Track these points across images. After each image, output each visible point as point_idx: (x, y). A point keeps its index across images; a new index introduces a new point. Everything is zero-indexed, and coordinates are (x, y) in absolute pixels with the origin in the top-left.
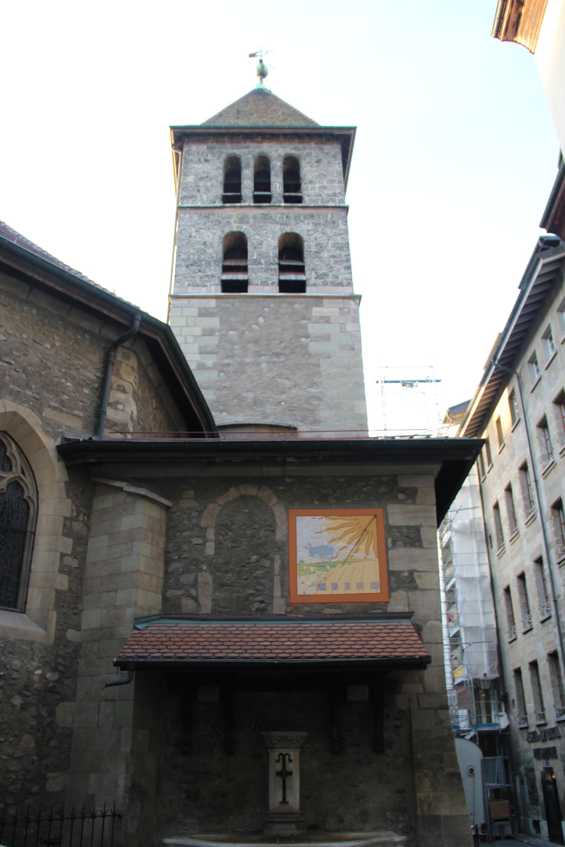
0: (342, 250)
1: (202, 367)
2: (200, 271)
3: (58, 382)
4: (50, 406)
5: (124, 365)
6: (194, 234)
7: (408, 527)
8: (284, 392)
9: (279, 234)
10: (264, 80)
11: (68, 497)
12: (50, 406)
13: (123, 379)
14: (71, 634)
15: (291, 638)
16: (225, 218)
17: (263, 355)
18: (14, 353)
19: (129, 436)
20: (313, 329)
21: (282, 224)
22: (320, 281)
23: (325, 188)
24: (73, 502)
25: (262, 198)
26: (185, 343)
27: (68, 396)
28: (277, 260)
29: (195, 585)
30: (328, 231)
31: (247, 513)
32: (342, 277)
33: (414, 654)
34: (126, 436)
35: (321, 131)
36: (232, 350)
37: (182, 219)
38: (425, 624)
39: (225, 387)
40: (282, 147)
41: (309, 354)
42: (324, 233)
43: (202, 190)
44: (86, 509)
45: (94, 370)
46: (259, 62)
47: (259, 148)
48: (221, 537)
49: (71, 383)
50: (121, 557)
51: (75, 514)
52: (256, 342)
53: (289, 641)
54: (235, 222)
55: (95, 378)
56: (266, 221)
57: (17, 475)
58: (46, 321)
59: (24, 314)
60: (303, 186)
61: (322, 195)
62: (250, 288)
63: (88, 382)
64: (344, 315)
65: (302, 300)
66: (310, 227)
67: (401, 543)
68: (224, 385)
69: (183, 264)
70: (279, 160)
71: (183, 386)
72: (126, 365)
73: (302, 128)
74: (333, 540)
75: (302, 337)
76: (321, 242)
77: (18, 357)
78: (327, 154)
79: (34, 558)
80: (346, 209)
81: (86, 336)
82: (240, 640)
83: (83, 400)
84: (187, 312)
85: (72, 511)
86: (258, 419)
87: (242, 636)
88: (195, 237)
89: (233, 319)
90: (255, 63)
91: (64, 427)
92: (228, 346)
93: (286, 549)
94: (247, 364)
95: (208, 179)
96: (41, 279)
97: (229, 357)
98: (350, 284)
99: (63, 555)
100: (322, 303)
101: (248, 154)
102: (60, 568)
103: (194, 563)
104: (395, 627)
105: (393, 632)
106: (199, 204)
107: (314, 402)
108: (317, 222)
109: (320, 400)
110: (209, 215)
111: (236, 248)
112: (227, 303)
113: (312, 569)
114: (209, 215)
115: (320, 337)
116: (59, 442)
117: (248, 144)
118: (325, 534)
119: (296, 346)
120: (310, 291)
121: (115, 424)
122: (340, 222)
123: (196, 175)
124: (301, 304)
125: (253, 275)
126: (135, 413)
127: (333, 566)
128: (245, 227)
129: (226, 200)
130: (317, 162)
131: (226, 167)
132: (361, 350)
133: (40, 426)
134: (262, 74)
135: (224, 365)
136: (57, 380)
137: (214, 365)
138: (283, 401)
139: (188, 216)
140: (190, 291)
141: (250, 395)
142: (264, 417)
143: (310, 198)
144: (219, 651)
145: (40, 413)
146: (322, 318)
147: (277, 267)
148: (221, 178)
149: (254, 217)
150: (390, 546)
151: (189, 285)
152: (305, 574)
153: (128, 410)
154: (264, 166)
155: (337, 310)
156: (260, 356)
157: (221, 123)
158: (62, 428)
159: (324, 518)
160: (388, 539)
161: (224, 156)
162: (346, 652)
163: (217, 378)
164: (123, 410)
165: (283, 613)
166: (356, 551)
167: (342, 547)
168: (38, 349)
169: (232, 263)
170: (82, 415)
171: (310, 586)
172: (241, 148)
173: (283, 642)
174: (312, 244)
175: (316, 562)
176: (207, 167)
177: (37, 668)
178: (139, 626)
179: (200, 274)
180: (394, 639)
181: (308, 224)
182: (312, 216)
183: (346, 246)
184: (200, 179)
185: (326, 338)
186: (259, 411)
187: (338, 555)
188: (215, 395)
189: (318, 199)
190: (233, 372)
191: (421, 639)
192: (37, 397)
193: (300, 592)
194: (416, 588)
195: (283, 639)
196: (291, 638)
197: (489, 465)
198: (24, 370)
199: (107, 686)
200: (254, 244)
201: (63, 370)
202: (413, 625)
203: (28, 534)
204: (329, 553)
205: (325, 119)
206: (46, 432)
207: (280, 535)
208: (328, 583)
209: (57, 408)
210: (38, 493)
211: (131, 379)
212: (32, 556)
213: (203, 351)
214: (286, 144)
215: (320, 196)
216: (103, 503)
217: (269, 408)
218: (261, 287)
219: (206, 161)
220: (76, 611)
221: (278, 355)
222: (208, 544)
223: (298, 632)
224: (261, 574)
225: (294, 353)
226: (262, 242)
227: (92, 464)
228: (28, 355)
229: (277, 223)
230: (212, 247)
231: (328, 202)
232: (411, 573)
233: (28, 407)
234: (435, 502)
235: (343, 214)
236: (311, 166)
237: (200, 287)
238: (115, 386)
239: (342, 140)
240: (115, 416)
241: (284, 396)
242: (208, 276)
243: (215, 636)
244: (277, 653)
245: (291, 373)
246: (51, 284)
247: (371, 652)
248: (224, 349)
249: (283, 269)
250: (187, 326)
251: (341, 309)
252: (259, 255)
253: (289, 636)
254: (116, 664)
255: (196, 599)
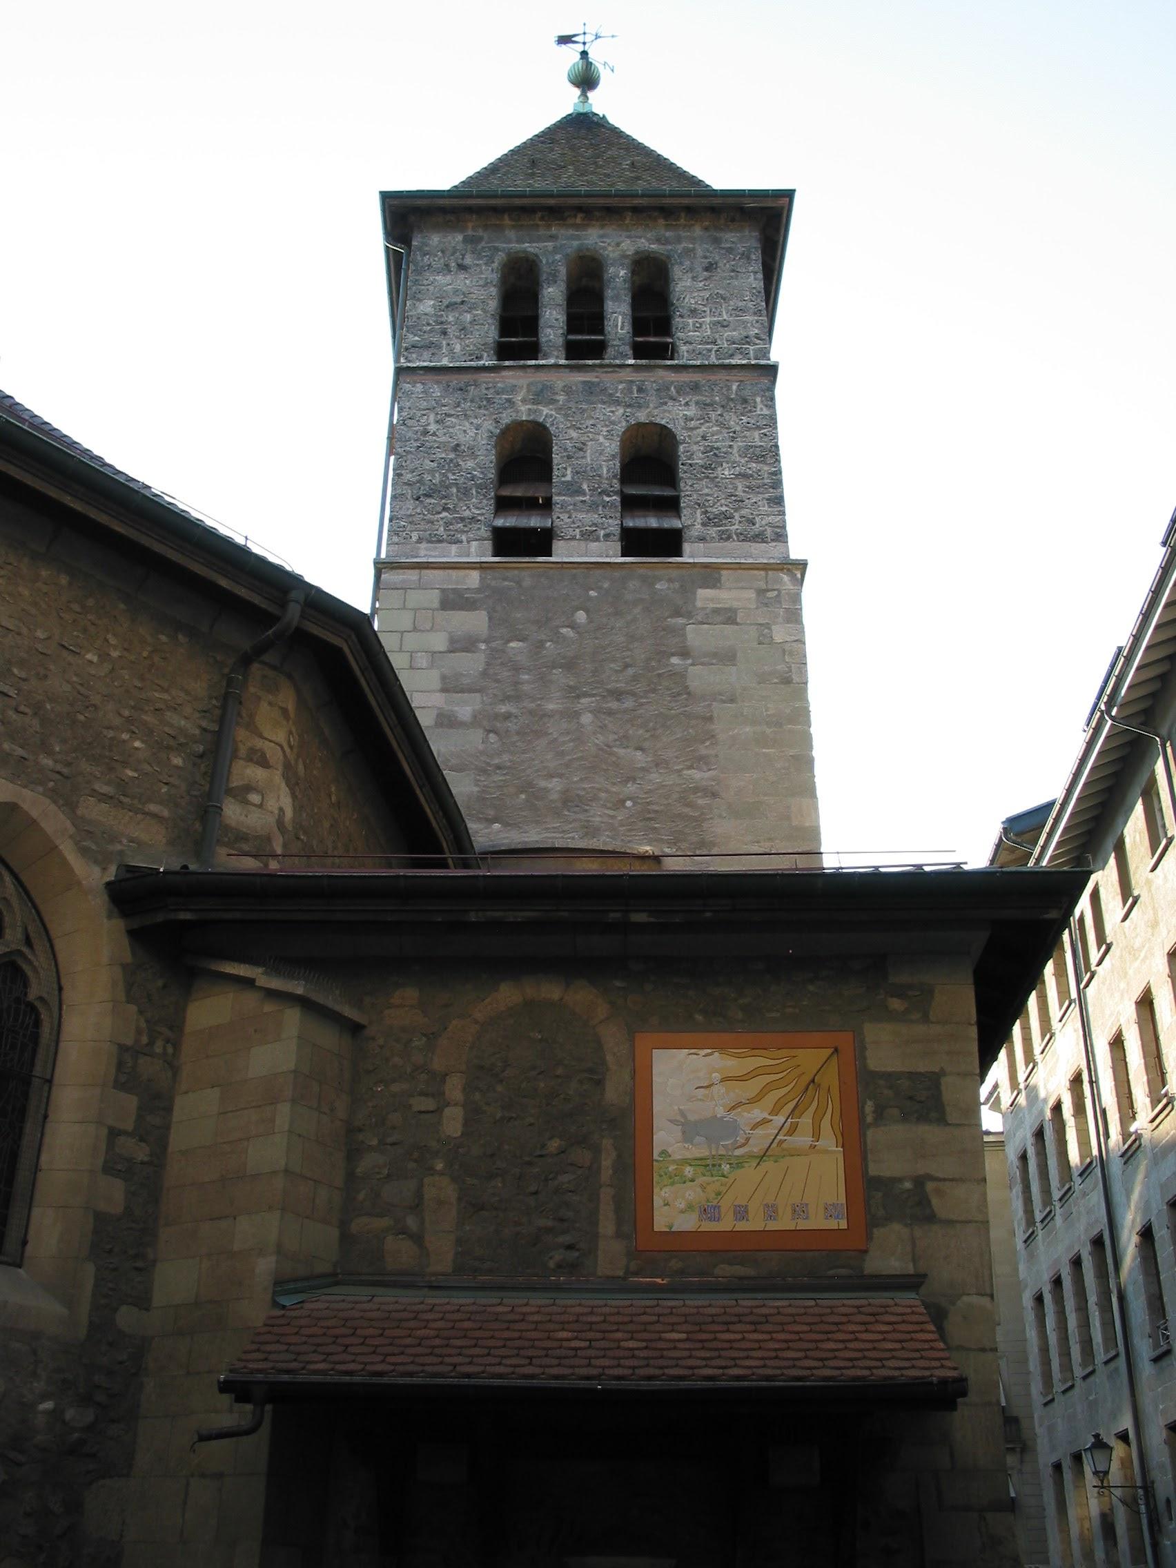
0: (764, 462)
1: (447, 721)
2: (445, 509)
3: (112, 739)
4: (94, 793)
5: (264, 706)
6: (433, 428)
7: (912, 1076)
8: (634, 779)
9: (621, 427)
10: (590, 94)
11: (130, 999)
12: (94, 793)
13: (262, 737)
14: (126, 1317)
15: (637, 1332)
16: (503, 391)
17: (586, 695)
18: (15, 671)
19: (274, 865)
20: (695, 635)
21: (629, 406)
22: (713, 531)
23: (724, 325)
24: (141, 1012)
25: (585, 345)
26: (411, 668)
27: (136, 770)
28: (617, 486)
29: (417, 1206)
30: (733, 420)
31: (541, 1040)
32: (764, 523)
33: (927, 1373)
34: (266, 865)
35: (716, 201)
36: (516, 683)
37: (408, 394)
38: (954, 1304)
39: (499, 767)
40: (629, 237)
41: (689, 693)
42: (721, 425)
43: (452, 331)
44: (171, 1028)
45: (198, 715)
46: (579, 56)
47: (578, 238)
48: (477, 1096)
49: (143, 742)
50: (248, 1139)
51: (145, 1040)
52: (570, 665)
53: (632, 1339)
54: (524, 401)
55: (197, 732)
56: (594, 399)
57: (14, 947)
58: (90, 602)
59: (39, 584)
60: (677, 321)
61: (719, 342)
62: (557, 546)
63: (182, 740)
64: (766, 605)
65: (674, 573)
66: (691, 411)
67: (896, 1112)
68: (496, 761)
69: (408, 492)
70: (622, 265)
71: (400, 755)
72: (270, 704)
73: (672, 195)
74: (739, 1104)
75: (673, 655)
76: (716, 445)
77: (25, 680)
78: (730, 250)
79: (47, 1139)
80: (772, 370)
81: (180, 637)
82: (516, 1335)
83: (171, 780)
84: (415, 598)
85: (139, 1032)
86: (573, 838)
87: (523, 1326)
88: (434, 434)
89: (519, 615)
90: (571, 55)
91: (125, 841)
92: (505, 674)
93: (629, 1123)
94: (550, 715)
95: (465, 307)
96: (78, 506)
97: (506, 699)
98: (780, 536)
99: (114, 1133)
100: (719, 580)
101: (554, 250)
102: (106, 1162)
103: (416, 1155)
104: (883, 1310)
105: (877, 1321)
106: (445, 362)
107: (700, 802)
108: (708, 401)
109: (714, 795)
110: (468, 384)
111: (525, 460)
112: (505, 579)
113: (688, 1171)
114: (468, 384)
115: (715, 655)
116: (111, 875)
117: (554, 231)
118: (719, 1090)
119: (659, 675)
120: (692, 553)
121: (242, 837)
122: (758, 399)
123: (440, 299)
124: (670, 580)
125: (564, 517)
126: (289, 813)
127: (738, 1164)
128: (545, 411)
129: (504, 351)
130: (707, 269)
131: (504, 280)
132: (806, 683)
133: (71, 837)
134: (586, 80)
135: (496, 716)
136: (111, 734)
137: (475, 717)
138: (630, 799)
139: (419, 387)
140: (422, 553)
141: (555, 785)
142: (586, 834)
143: (691, 347)
144: (468, 1360)
145: (70, 806)
146: (716, 611)
147: (616, 498)
148: (493, 305)
149: (568, 390)
150: (869, 1119)
151: (420, 540)
152: (673, 1184)
153: (272, 804)
154: (588, 288)
155: (752, 594)
156: (578, 697)
157: (495, 184)
158: (120, 842)
159: (716, 1054)
160: (865, 1103)
161: (500, 257)
162: (764, 1366)
163: (481, 747)
164: (260, 806)
165: (621, 1273)
166: (792, 1132)
167: (759, 1123)
168: (70, 664)
169: (518, 491)
170: (166, 813)
171: (682, 1212)
172: (539, 239)
173: (619, 1341)
174: (695, 448)
175: (698, 1156)
176: (463, 282)
177: (44, 1397)
178: (286, 1301)
179: (445, 514)
180: (880, 1337)
181: (687, 404)
182: (696, 388)
183: (774, 452)
184: (447, 307)
185: (727, 657)
186: (575, 820)
187: (748, 1139)
188: (477, 785)
189: (710, 351)
190: (518, 733)
191: (943, 1338)
192: (65, 771)
193: (660, 1224)
194: (931, 1218)
195: (619, 1335)
196: (637, 1332)
197: (1099, 949)
198: (38, 709)
199: (203, 1438)
200: (566, 450)
201: (126, 713)
202: (926, 1306)
203: (36, 1082)
204: (722, 1126)
205: (722, 171)
206: (84, 852)
207: (612, 1094)
208: (726, 1203)
209: (111, 798)
210: (60, 989)
211: (280, 736)
212: (42, 1134)
213: (450, 686)
214: (640, 231)
215: (714, 343)
216: (209, 1011)
217: (597, 815)
218: (583, 544)
219: (462, 267)
220: (140, 1264)
221: (618, 695)
222: (448, 1111)
223: (655, 1318)
224: (569, 1182)
225: (654, 691)
226: (584, 444)
227: (184, 925)
228: (46, 676)
229: (618, 402)
230: (473, 456)
231: (731, 356)
232: (920, 1181)
233: (43, 794)
234: (974, 1018)
235: (766, 381)
236: (693, 278)
237: (444, 545)
238: (243, 751)
239: (762, 220)
240: (242, 818)
241: (631, 788)
242: (462, 519)
243: (458, 1325)
244: (604, 1368)
245: (647, 735)
246: (103, 518)
247: (824, 1367)
248: (498, 681)
249: (630, 504)
250: (415, 629)
251: (761, 592)
252: (577, 473)
253: (630, 1327)
254: (225, 1387)
255: (418, 1239)
